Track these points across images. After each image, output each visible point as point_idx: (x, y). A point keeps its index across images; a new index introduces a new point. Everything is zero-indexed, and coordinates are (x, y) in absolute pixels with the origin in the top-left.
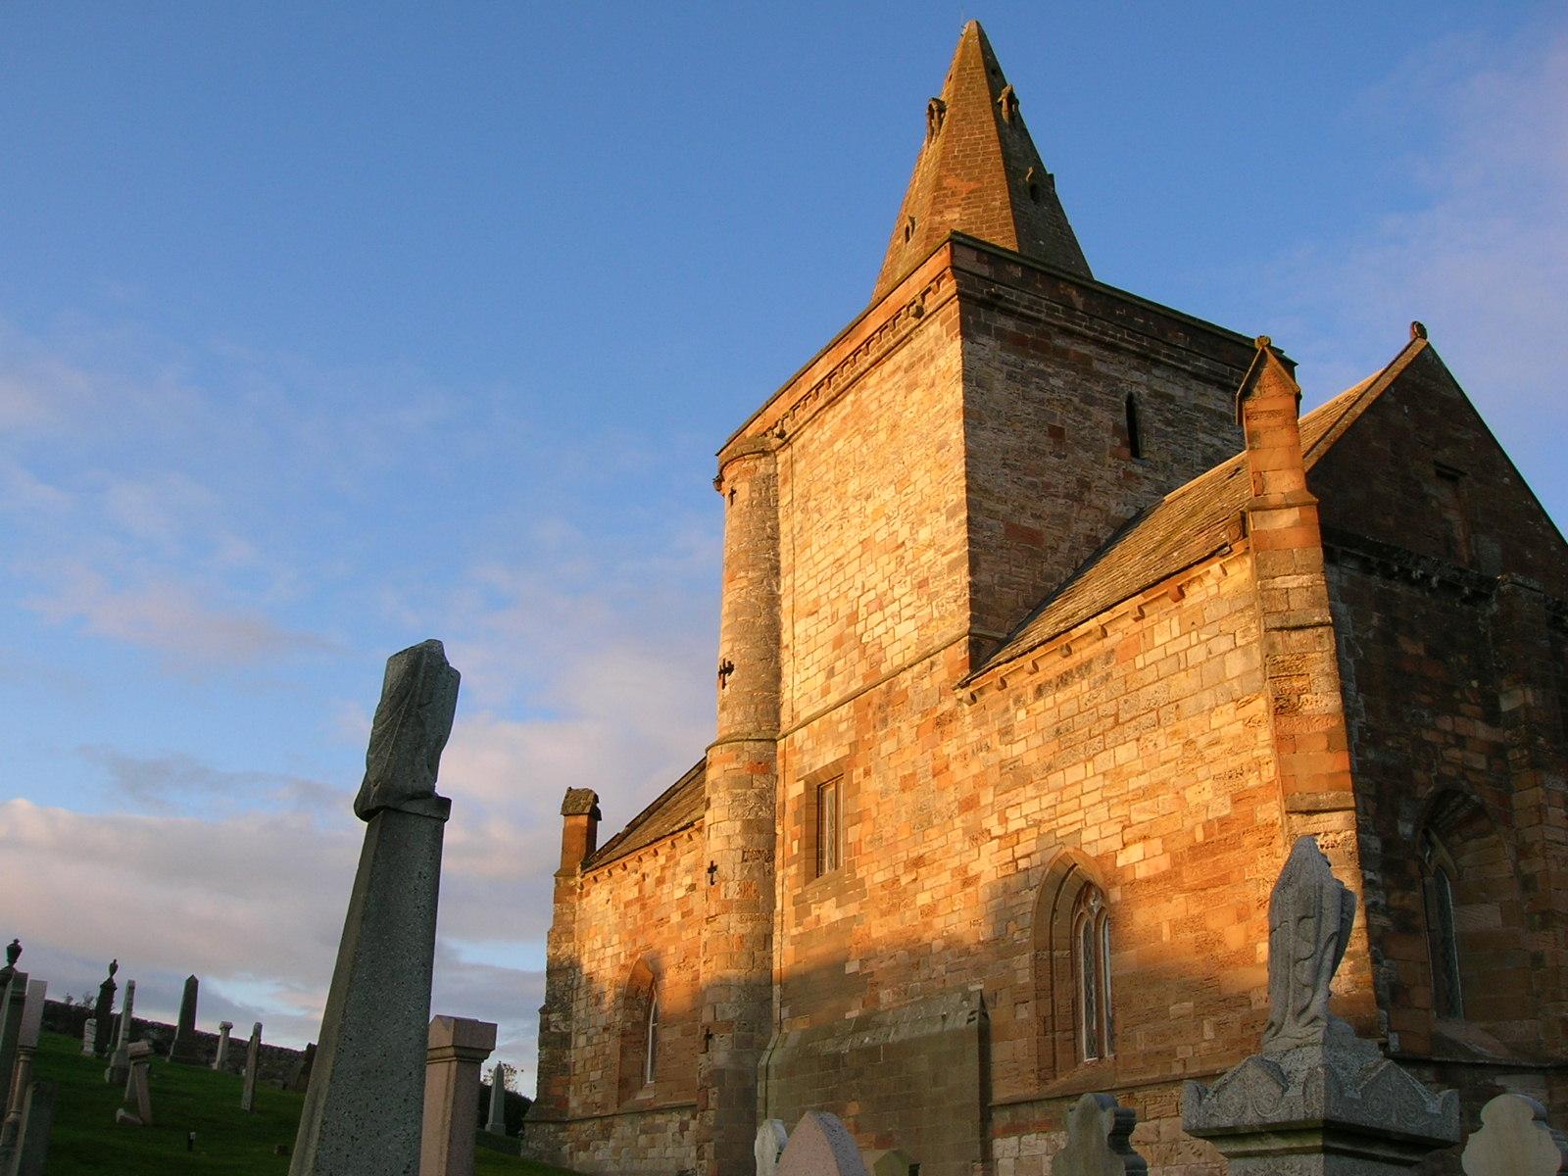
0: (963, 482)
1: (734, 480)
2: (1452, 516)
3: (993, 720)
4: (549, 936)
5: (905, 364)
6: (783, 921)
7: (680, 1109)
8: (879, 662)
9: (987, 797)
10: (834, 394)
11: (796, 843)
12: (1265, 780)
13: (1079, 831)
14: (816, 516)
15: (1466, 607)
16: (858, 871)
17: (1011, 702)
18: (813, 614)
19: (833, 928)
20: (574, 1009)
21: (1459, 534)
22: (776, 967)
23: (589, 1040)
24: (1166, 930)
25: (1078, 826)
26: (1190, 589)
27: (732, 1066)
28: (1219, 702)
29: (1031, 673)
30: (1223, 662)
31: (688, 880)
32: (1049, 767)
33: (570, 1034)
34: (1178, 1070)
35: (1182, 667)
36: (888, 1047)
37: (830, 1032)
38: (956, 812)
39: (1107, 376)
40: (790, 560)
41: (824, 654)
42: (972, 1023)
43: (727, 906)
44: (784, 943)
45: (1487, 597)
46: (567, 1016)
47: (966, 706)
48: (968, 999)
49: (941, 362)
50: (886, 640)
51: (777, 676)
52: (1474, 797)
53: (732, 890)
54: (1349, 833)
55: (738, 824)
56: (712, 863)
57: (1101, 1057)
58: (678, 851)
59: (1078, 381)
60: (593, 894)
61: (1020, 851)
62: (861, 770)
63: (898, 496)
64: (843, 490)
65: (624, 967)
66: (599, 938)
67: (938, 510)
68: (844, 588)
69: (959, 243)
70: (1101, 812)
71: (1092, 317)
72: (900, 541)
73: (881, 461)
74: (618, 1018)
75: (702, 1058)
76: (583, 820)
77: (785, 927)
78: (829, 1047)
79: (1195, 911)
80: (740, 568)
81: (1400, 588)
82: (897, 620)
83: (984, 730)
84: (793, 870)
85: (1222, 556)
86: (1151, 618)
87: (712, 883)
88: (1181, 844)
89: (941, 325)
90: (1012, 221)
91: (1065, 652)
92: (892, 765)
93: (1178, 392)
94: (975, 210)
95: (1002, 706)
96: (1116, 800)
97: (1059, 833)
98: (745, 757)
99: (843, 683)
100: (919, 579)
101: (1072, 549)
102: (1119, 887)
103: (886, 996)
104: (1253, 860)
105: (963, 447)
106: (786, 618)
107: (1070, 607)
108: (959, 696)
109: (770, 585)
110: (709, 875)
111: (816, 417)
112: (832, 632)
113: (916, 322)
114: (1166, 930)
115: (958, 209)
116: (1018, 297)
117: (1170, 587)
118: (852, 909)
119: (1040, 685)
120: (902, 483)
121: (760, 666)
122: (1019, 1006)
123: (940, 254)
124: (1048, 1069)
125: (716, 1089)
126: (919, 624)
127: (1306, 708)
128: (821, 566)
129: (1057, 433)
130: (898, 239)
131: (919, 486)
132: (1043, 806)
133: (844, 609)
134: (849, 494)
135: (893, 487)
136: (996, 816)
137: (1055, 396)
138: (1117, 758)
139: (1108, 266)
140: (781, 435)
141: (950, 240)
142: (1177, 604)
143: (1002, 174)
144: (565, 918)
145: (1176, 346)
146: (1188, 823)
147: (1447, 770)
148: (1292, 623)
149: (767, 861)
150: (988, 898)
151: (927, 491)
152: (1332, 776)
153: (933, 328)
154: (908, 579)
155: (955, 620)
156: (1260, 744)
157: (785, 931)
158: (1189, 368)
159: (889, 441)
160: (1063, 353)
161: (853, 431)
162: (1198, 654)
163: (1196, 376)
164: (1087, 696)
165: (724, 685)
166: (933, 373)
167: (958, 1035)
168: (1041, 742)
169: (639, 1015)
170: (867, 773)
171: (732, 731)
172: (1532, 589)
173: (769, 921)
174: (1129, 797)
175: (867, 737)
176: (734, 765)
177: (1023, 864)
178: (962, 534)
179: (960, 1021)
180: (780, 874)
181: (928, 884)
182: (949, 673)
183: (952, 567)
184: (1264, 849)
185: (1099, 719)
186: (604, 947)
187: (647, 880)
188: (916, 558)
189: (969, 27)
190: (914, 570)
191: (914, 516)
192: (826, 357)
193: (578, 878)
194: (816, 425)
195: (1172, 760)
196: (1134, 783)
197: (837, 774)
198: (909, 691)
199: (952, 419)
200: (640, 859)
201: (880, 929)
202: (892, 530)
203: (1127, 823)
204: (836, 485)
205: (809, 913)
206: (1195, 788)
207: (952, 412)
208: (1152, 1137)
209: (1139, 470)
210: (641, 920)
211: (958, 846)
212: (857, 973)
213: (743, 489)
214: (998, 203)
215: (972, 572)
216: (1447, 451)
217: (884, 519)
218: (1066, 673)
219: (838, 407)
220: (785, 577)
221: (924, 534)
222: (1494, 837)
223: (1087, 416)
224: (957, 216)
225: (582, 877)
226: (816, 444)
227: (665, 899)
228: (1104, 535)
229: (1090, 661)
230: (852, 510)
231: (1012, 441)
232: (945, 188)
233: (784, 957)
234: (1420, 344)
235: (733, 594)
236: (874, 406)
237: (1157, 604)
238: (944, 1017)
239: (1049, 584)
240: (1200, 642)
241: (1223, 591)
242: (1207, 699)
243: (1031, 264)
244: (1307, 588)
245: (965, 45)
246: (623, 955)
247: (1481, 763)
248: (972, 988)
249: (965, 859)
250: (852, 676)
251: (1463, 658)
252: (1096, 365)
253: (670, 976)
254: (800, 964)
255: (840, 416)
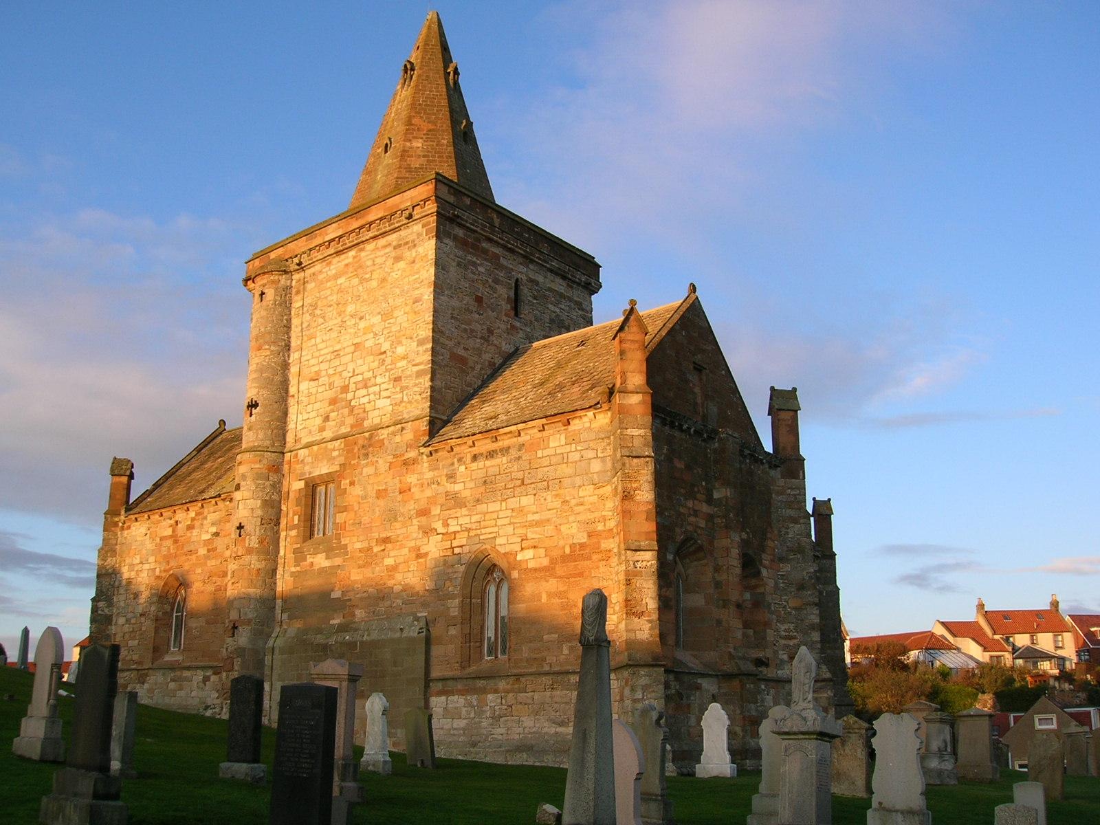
0: (431, 326)
1: (264, 286)
2: (697, 390)
3: (443, 468)
4: (99, 552)
5: (394, 243)
6: (285, 562)
7: (203, 668)
8: (363, 419)
9: (436, 511)
10: (341, 248)
11: (296, 518)
12: (607, 528)
13: (495, 538)
14: (321, 320)
15: (703, 444)
16: (342, 540)
17: (456, 460)
18: (314, 380)
19: (322, 571)
20: (115, 600)
21: (699, 401)
22: (279, 589)
23: (128, 621)
24: (544, 597)
25: (494, 535)
26: (574, 421)
27: (250, 646)
28: (585, 483)
29: (470, 447)
30: (589, 463)
31: (214, 529)
32: (478, 500)
33: (111, 616)
34: (547, 668)
35: (565, 461)
36: (362, 643)
37: (319, 631)
38: (414, 515)
39: (507, 267)
40: (299, 343)
41: (323, 407)
42: (420, 634)
43: (249, 551)
44: (285, 575)
45: (714, 439)
46: (110, 604)
47: (425, 457)
48: (418, 620)
49: (420, 250)
50: (368, 407)
51: (286, 413)
52: (699, 541)
53: (253, 542)
54: (653, 562)
55: (259, 502)
56: (240, 523)
57: (496, 657)
58: (206, 510)
59: (492, 269)
60: (133, 528)
61: (455, 543)
62: (348, 481)
63: (383, 323)
64: (343, 309)
65: (158, 578)
66: (138, 557)
67: (411, 338)
68: (339, 369)
69: (440, 181)
70: (510, 529)
71: (503, 232)
72: (383, 350)
73: (372, 299)
74: (153, 608)
75: (229, 640)
76: (125, 479)
77: (286, 566)
78: (320, 639)
79: (561, 589)
80: (266, 343)
81: (677, 433)
82: (378, 396)
83: (436, 473)
84: (294, 533)
85: (596, 409)
86: (549, 431)
87: (240, 536)
88: (556, 553)
89: (423, 227)
90: (453, 155)
91: (494, 439)
92: (371, 482)
93: (540, 279)
94: (431, 143)
95: (450, 461)
96: (519, 525)
97: (481, 537)
98: (265, 462)
99: (336, 427)
100: (395, 376)
101: (481, 369)
102: (517, 571)
103: (359, 613)
104: (598, 567)
105: (432, 305)
106: (293, 379)
107: (488, 409)
108: (422, 451)
109: (284, 356)
110: (238, 531)
111: (326, 259)
112: (330, 394)
113: (406, 221)
114: (544, 597)
115: (421, 140)
116: (467, 217)
117: (564, 418)
118: (338, 561)
119: (475, 455)
120: (386, 316)
121: (276, 406)
122: (450, 627)
123: (428, 185)
124: (466, 661)
125: (240, 659)
126: (393, 402)
127: (637, 498)
128: (322, 352)
129: (479, 300)
130: (379, 148)
131: (399, 320)
132: (472, 521)
133: (338, 383)
134: (348, 313)
135: (380, 316)
136: (441, 522)
137: (480, 278)
138: (521, 502)
139: (505, 197)
140: (300, 264)
141: (435, 179)
142: (565, 428)
143: (449, 122)
144: (111, 541)
145: (543, 252)
146: (562, 543)
147: (690, 528)
148: (634, 454)
149: (275, 525)
150: (433, 566)
151: (405, 325)
152: (649, 533)
153: (417, 228)
154: (387, 374)
155: (418, 404)
156: (607, 509)
157: (286, 568)
158: (548, 266)
159: (379, 288)
160: (485, 252)
161: (352, 274)
162: (575, 456)
163: (551, 271)
164: (505, 466)
165: (251, 415)
166: (414, 255)
167: (411, 640)
168: (474, 486)
169: (167, 607)
170: (352, 483)
171: (256, 444)
172: (735, 437)
173: (275, 562)
174: (527, 524)
175: (353, 462)
176: (258, 466)
177: (457, 551)
178: (428, 357)
179: (413, 632)
180: (283, 534)
181: (392, 554)
182: (415, 436)
183: (419, 374)
184: (604, 562)
185: (512, 480)
186: (141, 563)
187: (179, 525)
188: (393, 363)
189: (431, 15)
190: (392, 369)
191: (394, 337)
192: (337, 223)
193: (122, 518)
194: (324, 264)
195: (555, 509)
196: (530, 517)
197: (328, 479)
198: (385, 441)
199: (426, 286)
200: (175, 511)
201: (357, 576)
202: (377, 342)
203: (525, 538)
204: (338, 305)
205: (305, 560)
206: (567, 526)
207: (426, 282)
208: (530, 701)
209: (518, 324)
210: (174, 549)
211: (415, 535)
212: (340, 598)
213: (270, 293)
214: (445, 142)
215: (432, 379)
216: (699, 356)
217: (372, 334)
218: (493, 451)
219: (343, 257)
220: (294, 353)
221: (400, 350)
222: (705, 561)
223: (495, 290)
224: (420, 145)
225: (126, 517)
226: (324, 275)
227: (194, 539)
228: (498, 361)
229: (509, 447)
230: (348, 323)
231: (455, 303)
232: (413, 125)
233: (284, 583)
234: (693, 296)
235: (258, 359)
236: (369, 263)
237: (553, 425)
238: (401, 629)
239: (469, 388)
240: (576, 450)
241: (592, 426)
242: (578, 481)
243: (475, 197)
244: (642, 436)
245: (429, 28)
246: (158, 570)
247: (702, 524)
248: (419, 615)
249: (419, 543)
250: (343, 424)
251: (700, 470)
252: (502, 261)
253: (197, 586)
254: (297, 590)
255: (344, 263)
